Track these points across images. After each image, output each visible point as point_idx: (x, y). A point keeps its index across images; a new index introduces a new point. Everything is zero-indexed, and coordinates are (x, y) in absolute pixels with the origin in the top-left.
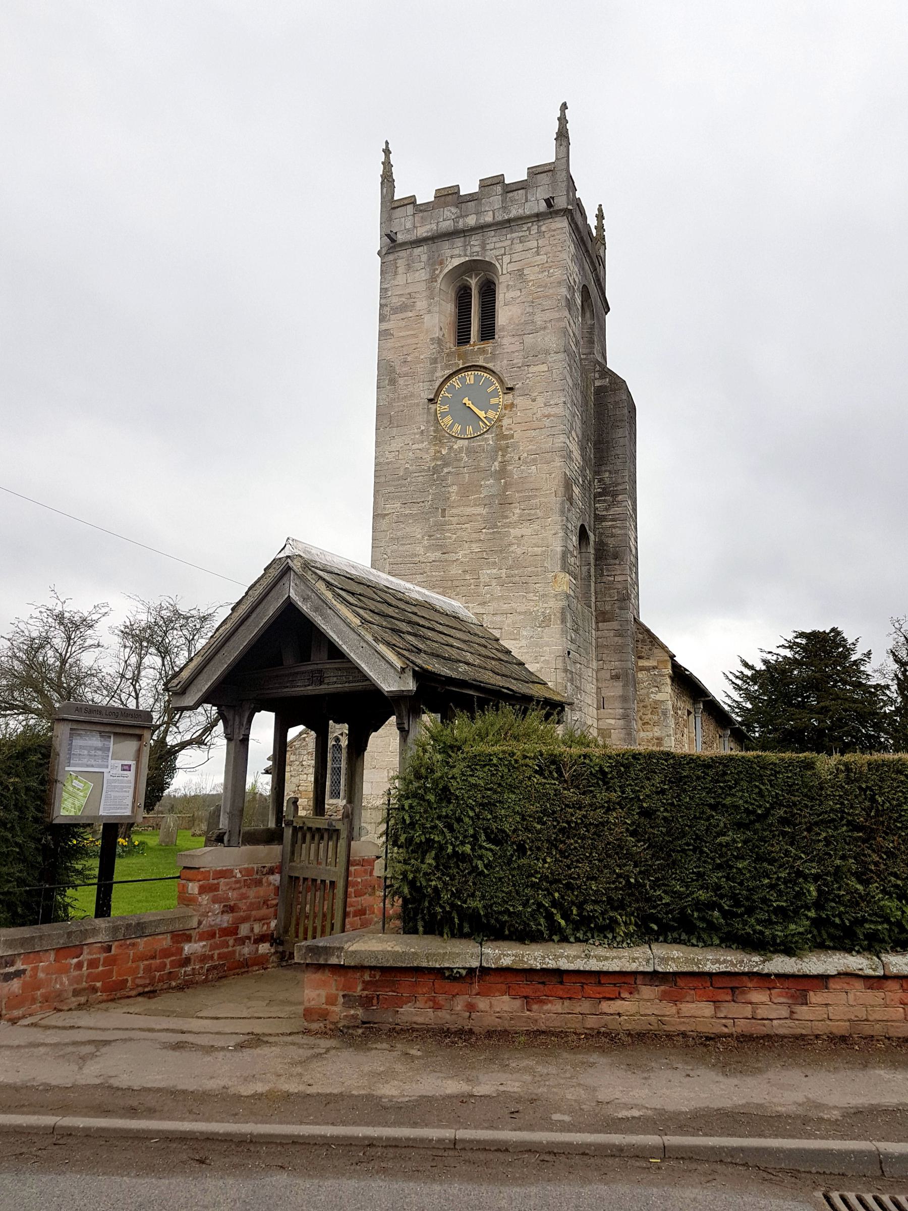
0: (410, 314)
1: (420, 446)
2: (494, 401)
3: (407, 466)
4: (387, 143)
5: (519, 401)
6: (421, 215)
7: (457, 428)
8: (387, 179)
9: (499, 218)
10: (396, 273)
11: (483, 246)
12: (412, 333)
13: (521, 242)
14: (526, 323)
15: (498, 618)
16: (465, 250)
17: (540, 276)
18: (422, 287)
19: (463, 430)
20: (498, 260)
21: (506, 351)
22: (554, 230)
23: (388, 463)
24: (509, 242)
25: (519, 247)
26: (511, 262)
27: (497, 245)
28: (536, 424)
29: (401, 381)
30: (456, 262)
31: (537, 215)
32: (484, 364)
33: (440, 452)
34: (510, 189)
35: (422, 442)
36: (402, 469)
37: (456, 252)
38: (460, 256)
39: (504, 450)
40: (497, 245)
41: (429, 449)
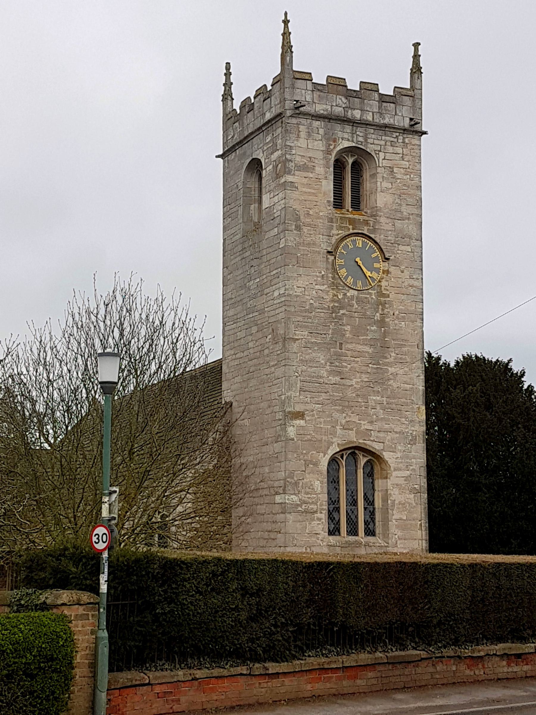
0: (311, 175)
1: (323, 288)
2: (376, 265)
3: (311, 301)
4: (286, 14)
5: (392, 269)
6: (318, 93)
7: (350, 280)
8: (287, 49)
9: (378, 120)
10: (298, 136)
11: (366, 138)
12: (313, 191)
13: (391, 146)
14: (396, 211)
15: (381, 435)
16: (353, 137)
17: (405, 177)
18: (320, 155)
19: (355, 283)
20: (376, 154)
21: (382, 228)
22: (414, 145)
23: (297, 296)
24: (383, 143)
25: (390, 149)
26: (384, 159)
27: (376, 142)
28: (404, 290)
29: (305, 229)
30: (346, 144)
31: (404, 130)
32: (368, 234)
33: (337, 296)
34: (383, 99)
35: (323, 285)
36: (308, 303)
37: (346, 136)
38: (348, 140)
39: (383, 304)
40: (376, 142)
41: (329, 291)
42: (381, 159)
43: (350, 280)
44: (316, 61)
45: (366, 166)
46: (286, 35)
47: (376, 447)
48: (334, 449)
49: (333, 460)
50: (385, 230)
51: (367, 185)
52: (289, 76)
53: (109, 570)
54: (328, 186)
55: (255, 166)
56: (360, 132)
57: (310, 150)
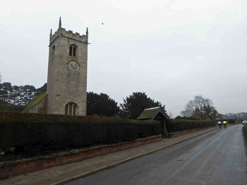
4: (60, 17)
7: (72, 69)
8: (60, 23)
19: (73, 70)
25: (81, 46)
30: (72, 43)
31: (84, 42)
34: (80, 36)
42: (79, 48)
43: (72, 69)
44: (67, 27)
45: (76, 48)
46: (60, 21)
47: (76, 102)
48: (67, 103)
49: (67, 106)
50: (80, 60)
51: (77, 52)
52: (61, 29)
53: (148, 136)
54: (68, 51)
55: (54, 47)
56: (75, 41)
57: (65, 44)
